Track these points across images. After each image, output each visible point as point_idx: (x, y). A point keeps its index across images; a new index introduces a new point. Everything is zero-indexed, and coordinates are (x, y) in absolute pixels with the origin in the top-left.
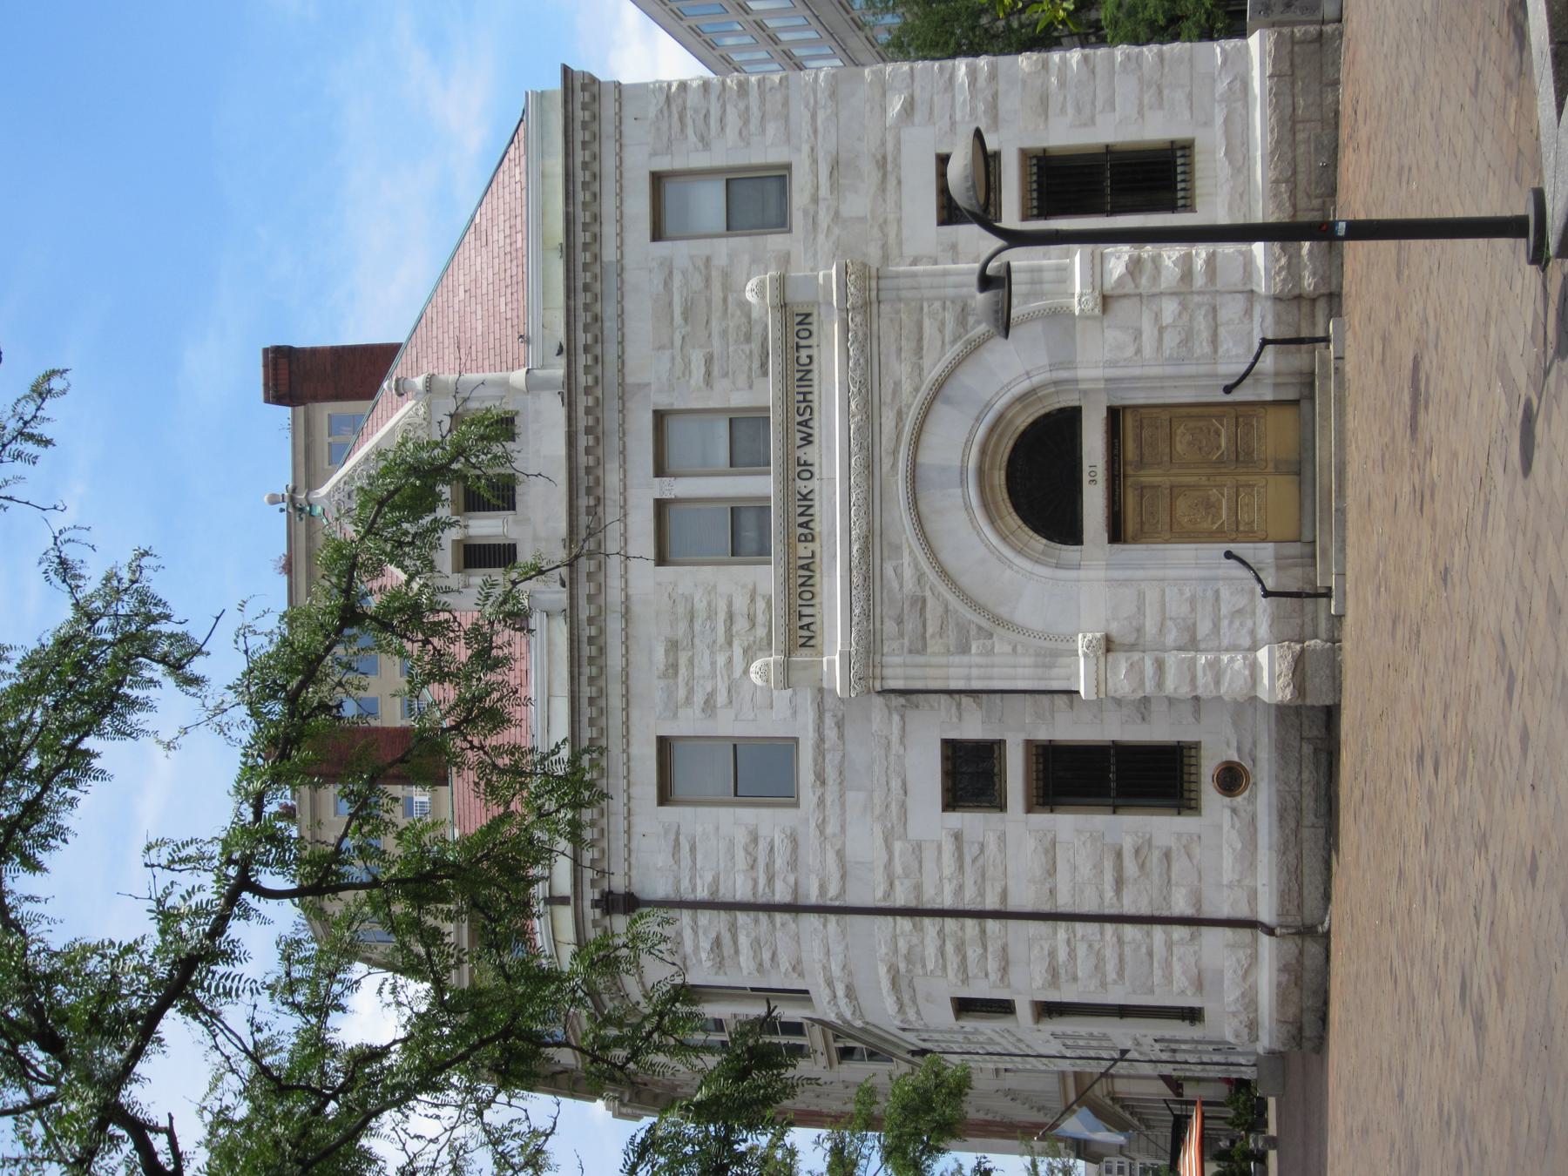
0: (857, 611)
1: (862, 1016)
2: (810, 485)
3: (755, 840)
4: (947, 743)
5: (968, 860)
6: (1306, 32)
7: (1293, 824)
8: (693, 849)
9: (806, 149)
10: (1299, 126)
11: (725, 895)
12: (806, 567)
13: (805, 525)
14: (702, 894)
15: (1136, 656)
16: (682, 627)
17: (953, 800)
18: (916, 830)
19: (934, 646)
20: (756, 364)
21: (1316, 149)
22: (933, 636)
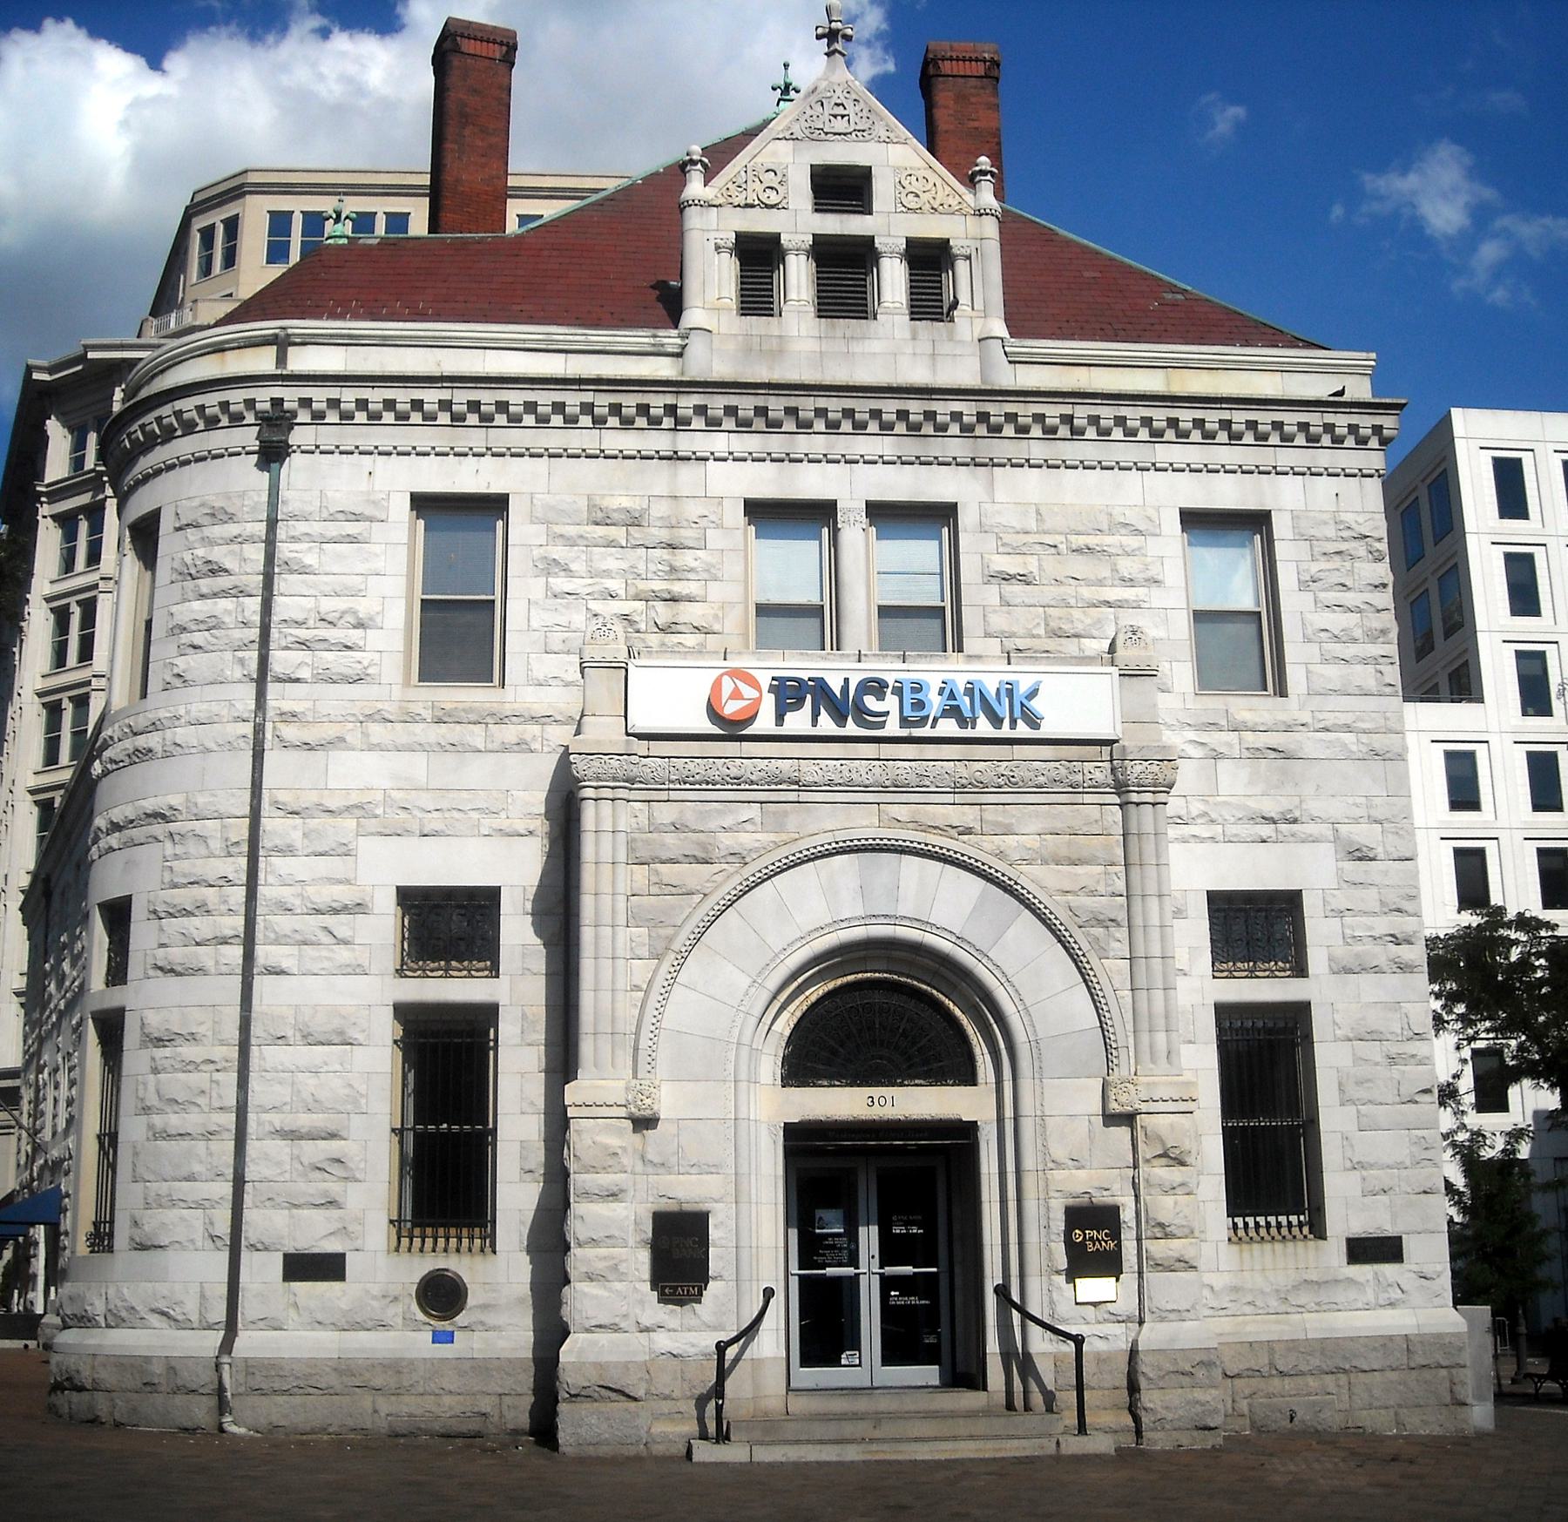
0: (691, 766)
1: (106, 773)
3: (361, 625)
5: (329, 920)
6: (1463, 1384)
7: (377, 1382)
8: (352, 539)
9: (1305, 717)
10: (1343, 1378)
11: (282, 583)
14: (284, 550)
17: (414, 901)
18: (368, 848)
21: (1314, 1403)
22: (657, 873)
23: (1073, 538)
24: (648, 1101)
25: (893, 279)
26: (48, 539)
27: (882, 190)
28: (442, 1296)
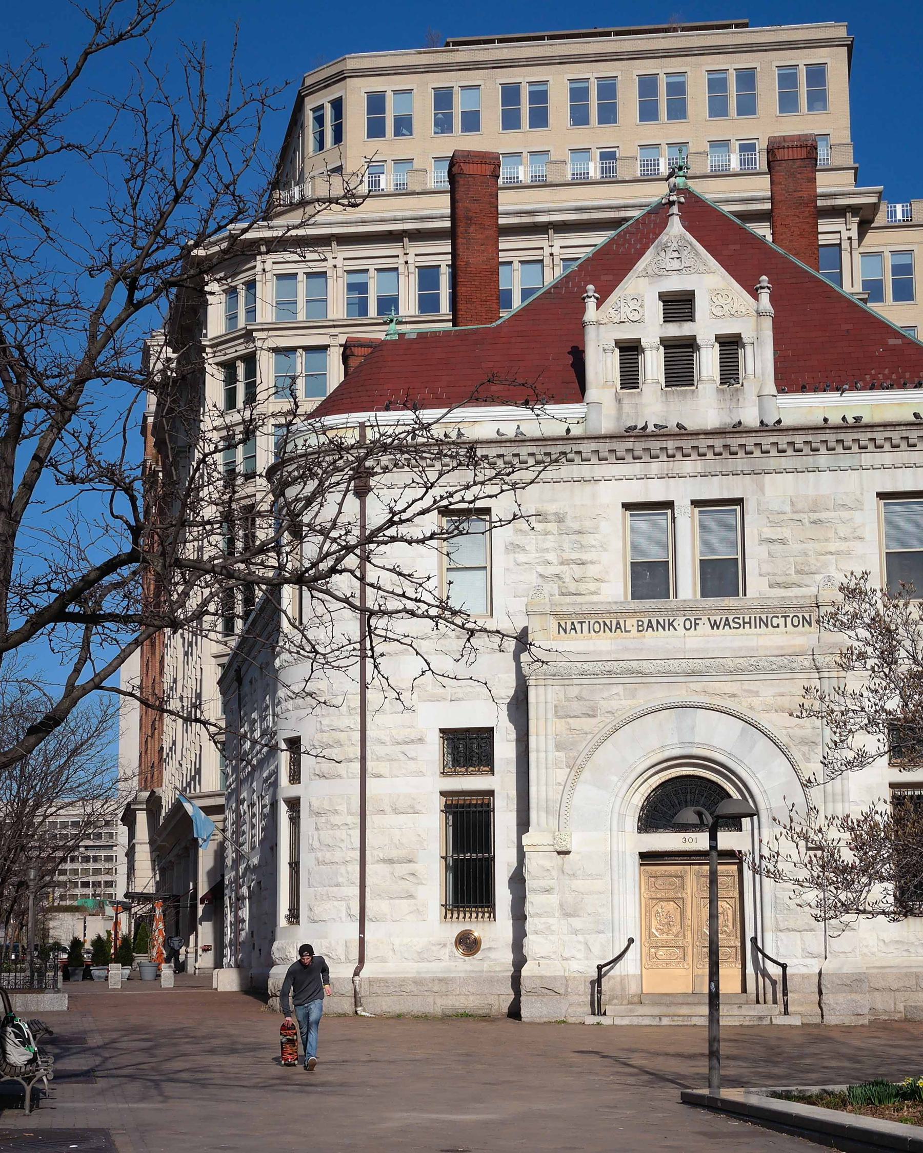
2: (681, 629)
4: (490, 730)
5: (405, 748)
12: (618, 626)
13: (650, 625)
15: (555, 873)
16: (576, 526)
19: (561, 725)
20: (780, 579)
23: (811, 514)
24: (564, 843)
25: (708, 361)
26: (214, 389)
27: (701, 305)
28: (468, 944)
